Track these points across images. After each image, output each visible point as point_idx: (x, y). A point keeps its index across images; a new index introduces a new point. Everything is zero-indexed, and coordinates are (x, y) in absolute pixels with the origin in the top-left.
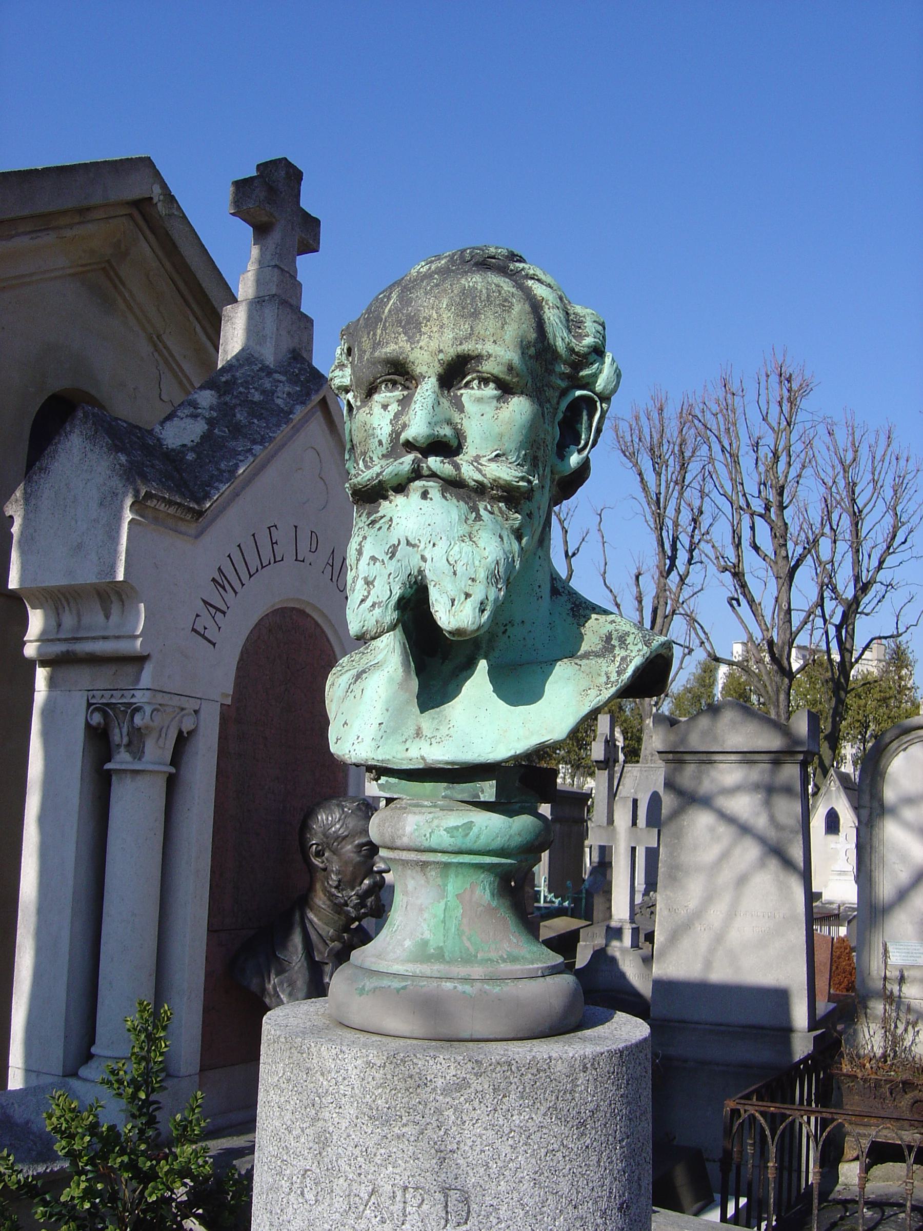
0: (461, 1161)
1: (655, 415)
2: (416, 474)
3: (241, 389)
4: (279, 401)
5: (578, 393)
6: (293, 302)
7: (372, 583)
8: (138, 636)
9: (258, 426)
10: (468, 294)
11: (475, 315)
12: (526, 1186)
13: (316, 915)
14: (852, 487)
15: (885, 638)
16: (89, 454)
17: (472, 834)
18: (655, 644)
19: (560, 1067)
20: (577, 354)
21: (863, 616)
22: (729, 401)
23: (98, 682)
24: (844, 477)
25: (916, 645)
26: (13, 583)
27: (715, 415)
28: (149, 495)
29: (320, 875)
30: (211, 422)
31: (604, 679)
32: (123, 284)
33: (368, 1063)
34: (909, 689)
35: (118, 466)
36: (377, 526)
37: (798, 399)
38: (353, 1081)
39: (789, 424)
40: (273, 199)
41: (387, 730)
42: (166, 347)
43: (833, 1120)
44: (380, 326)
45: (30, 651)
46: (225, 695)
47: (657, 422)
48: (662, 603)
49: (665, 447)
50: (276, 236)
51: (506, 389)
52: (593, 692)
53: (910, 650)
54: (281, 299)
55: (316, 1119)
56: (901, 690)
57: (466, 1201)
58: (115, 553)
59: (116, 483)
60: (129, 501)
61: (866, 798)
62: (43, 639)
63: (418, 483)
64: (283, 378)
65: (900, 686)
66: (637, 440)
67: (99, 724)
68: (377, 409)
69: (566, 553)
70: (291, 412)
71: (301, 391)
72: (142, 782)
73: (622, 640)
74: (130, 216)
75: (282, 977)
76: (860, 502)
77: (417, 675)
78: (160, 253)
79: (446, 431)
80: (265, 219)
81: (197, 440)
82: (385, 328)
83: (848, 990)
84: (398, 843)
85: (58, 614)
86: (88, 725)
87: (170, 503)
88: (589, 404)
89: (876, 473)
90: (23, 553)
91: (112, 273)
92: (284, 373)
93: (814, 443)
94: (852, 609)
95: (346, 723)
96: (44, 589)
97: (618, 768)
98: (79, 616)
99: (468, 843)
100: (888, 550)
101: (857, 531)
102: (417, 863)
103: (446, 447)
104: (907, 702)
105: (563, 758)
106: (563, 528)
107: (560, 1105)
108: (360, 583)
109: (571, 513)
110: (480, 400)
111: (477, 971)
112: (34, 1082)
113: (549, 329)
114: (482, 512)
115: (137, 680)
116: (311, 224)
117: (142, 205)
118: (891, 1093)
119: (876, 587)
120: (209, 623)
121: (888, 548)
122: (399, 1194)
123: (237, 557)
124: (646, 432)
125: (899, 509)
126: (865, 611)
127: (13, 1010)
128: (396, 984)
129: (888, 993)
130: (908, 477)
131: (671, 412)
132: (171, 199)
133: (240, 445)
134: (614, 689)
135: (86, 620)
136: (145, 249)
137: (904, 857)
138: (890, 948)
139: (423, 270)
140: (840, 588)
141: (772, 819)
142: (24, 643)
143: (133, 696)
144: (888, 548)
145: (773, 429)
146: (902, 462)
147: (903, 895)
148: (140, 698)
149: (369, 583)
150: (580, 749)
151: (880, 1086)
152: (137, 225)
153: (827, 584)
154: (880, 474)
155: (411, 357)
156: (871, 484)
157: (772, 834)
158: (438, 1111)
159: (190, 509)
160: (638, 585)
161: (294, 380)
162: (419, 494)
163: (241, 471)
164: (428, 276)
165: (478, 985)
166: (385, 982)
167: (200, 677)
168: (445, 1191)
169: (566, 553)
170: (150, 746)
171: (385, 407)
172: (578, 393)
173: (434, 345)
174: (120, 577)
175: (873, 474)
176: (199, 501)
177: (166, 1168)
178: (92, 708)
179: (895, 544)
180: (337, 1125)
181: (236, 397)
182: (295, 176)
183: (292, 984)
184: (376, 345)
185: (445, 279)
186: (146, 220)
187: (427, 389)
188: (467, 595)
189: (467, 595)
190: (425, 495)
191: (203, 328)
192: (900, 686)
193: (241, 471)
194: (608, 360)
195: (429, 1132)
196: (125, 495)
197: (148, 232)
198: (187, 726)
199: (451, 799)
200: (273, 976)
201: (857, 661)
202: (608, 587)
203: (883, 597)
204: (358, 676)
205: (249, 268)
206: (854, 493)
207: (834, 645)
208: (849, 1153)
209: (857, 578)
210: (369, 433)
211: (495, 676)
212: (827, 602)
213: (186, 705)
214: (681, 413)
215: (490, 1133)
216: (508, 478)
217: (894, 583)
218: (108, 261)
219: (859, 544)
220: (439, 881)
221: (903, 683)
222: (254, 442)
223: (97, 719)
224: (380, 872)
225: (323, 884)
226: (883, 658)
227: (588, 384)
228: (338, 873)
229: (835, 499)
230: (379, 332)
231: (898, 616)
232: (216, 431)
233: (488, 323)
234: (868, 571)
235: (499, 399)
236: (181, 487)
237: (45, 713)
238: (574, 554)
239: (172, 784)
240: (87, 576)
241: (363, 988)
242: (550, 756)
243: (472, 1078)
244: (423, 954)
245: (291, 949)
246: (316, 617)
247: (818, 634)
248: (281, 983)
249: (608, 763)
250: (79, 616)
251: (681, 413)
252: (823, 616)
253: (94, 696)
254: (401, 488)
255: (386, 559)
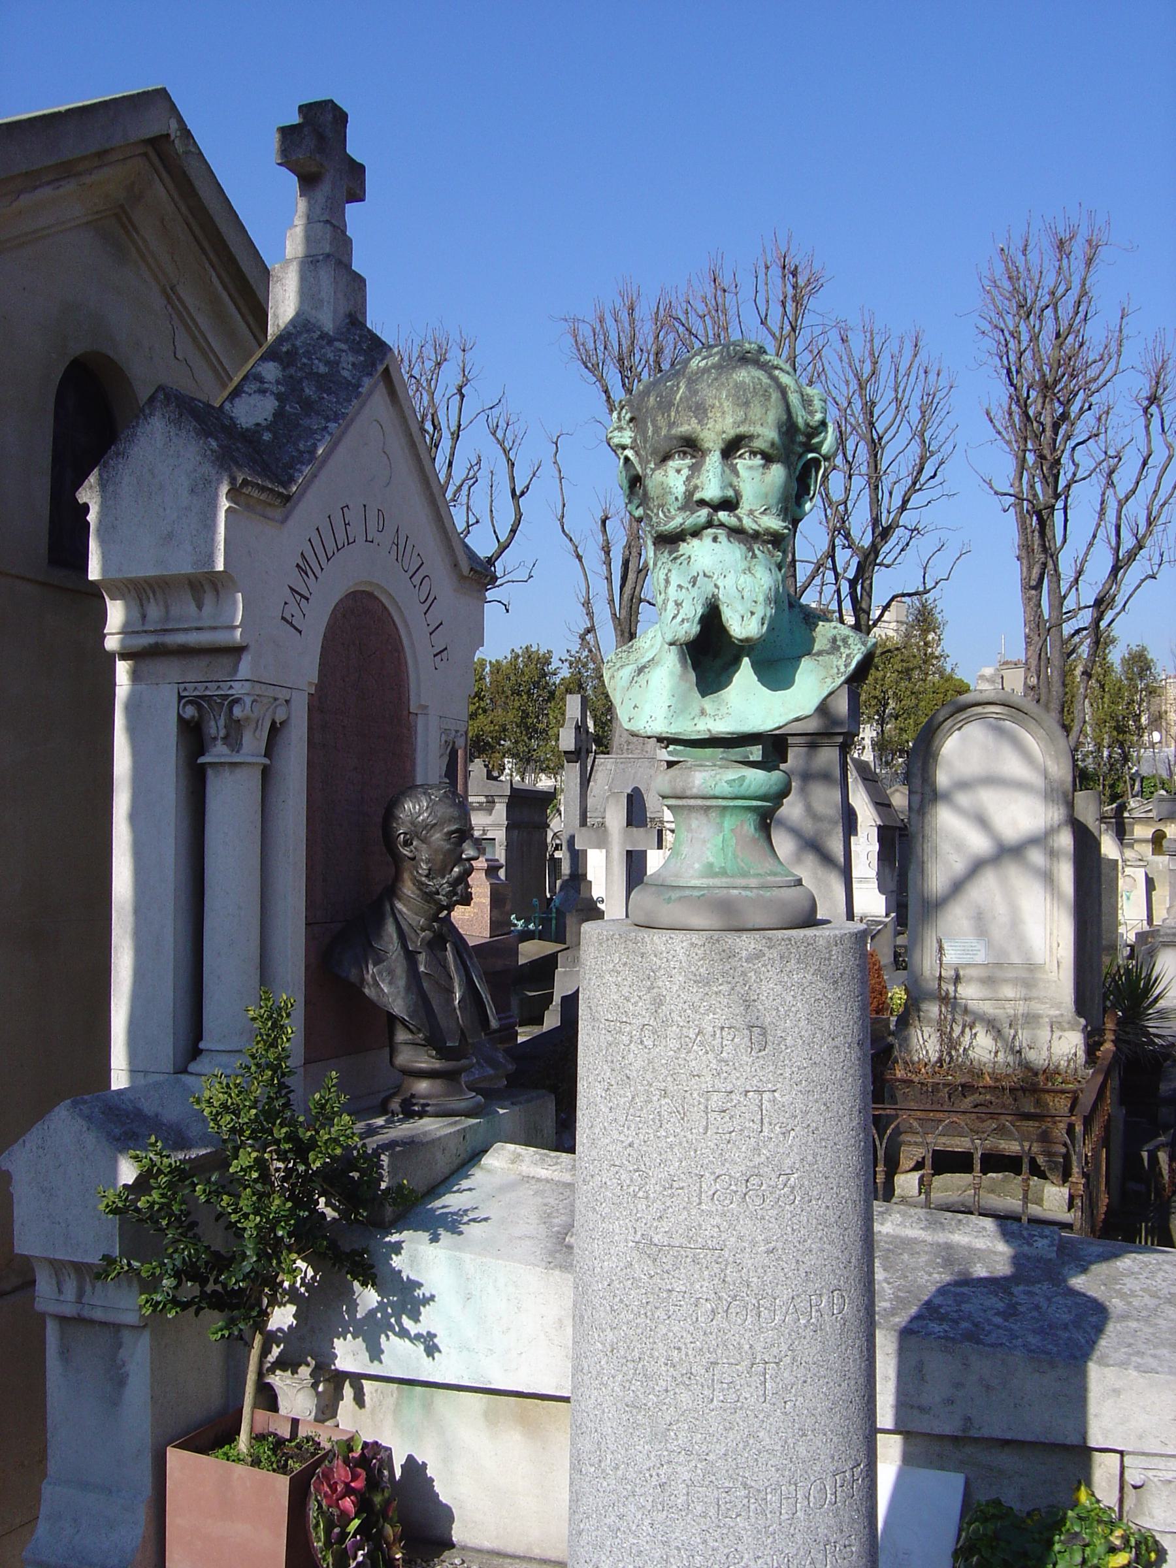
0: (760, 1007)
1: (624, 316)
2: (709, 524)
3: (305, 360)
4: (345, 373)
5: (810, 456)
6: (345, 259)
7: (681, 604)
8: (238, 627)
9: (329, 401)
10: (739, 386)
11: (747, 404)
12: (803, 1023)
13: (405, 905)
14: (869, 408)
15: (909, 595)
16: (174, 440)
17: (745, 784)
18: (869, 644)
19: (821, 942)
20: (811, 427)
21: (883, 568)
22: (720, 300)
23: (194, 673)
24: (861, 395)
25: (944, 603)
26: (94, 572)
27: (702, 317)
28: (245, 483)
29: (407, 864)
30: (279, 397)
31: (835, 670)
32: (137, 233)
33: (692, 944)
34: (937, 657)
35: (209, 452)
36: (679, 561)
37: (806, 298)
38: (681, 957)
39: (794, 329)
40: (318, 148)
41: (675, 712)
42: (179, 299)
43: (897, 1116)
44: (673, 410)
45: (112, 643)
46: (310, 683)
47: (627, 325)
48: (635, 553)
49: (637, 357)
50: (325, 188)
51: (768, 459)
52: (829, 680)
53: (938, 610)
54: (331, 257)
55: (650, 989)
56: (928, 659)
57: (764, 1034)
58: (212, 541)
59: (208, 469)
60: (224, 489)
61: (917, 781)
62: (126, 631)
63: (709, 530)
64: (344, 346)
65: (925, 654)
66: (602, 348)
67: (193, 717)
68: (672, 473)
69: (513, 491)
70: (360, 386)
71: (365, 361)
72: (240, 774)
73: (845, 640)
74: (145, 155)
75: (381, 966)
76: (880, 427)
77: (694, 669)
78: (176, 196)
79: (730, 493)
80: (314, 169)
81: (270, 418)
82: (677, 412)
83: (877, 1013)
84: (688, 793)
85: (142, 606)
86: (180, 718)
87: (263, 489)
88: (816, 463)
89: (900, 390)
90: (102, 542)
91: (124, 219)
92: (346, 342)
93: (823, 353)
94: (868, 561)
95: (636, 706)
96: (131, 580)
97: (590, 761)
98: (167, 607)
99: (742, 791)
100: (914, 488)
101: (876, 462)
102: (701, 807)
103: (729, 504)
104: (934, 673)
105: (509, 750)
106: (509, 460)
107: (823, 968)
108: (671, 605)
109: (518, 441)
110: (751, 468)
111: (753, 882)
112: (141, 1081)
113: (793, 410)
114: (757, 552)
115: (235, 669)
116: (357, 171)
117: (159, 143)
118: (950, 1098)
119: (899, 532)
120: (295, 610)
121: (914, 484)
122: (718, 1032)
123: (316, 541)
124: (613, 336)
125: (927, 435)
126: (885, 562)
127: (113, 1013)
128: (696, 893)
129: (943, 993)
130: (939, 395)
131: (645, 311)
132: (187, 134)
133: (315, 423)
134: (843, 678)
135: (175, 610)
136: (160, 192)
137: (959, 846)
138: (945, 946)
139: (702, 364)
140: (855, 533)
141: (809, 809)
142: (104, 636)
143: (231, 687)
144: (914, 484)
145: (773, 335)
146: (932, 376)
147: (958, 887)
148: (238, 690)
149: (678, 604)
150: (530, 739)
151: (938, 1091)
152: (152, 164)
153: (840, 529)
154: (904, 391)
155: (702, 436)
156: (894, 404)
157: (808, 827)
158: (744, 974)
159: (280, 494)
160: (604, 531)
161: (356, 349)
162: (710, 539)
163: (320, 452)
164: (706, 370)
165: (755, 891)
166: (687, 893)
167: (284, 666)
168: (750, 1027)
169: (513, 491)
170: (247, 738)
171: (678, 471)
172: (810, 456)
173: (718, 427)
174: (220, 566)
175: (896, 391)
176: (286, 484)
177: (327, 1137)
178: (183, 701)
179: (922, 479)
180: (669, 990)
181: (301, 369)
182: (340, 118)
183: (391, 972)
184: (671, 425)
185: (720, 374)
186: (162, 160)
187: (713, 460)
188: (752, 613)
189: (752, 613)
190: (715, 539)
191: (219, 277)
192: (925, 654)
193: (320, 452)
194: (830, 430)
195: (738, 988)
196: (219, 481)
197: (164, 175)
198: (280, 717)
199: (726, 759)
200: (370, 967)
201: (875, 625)
202: (566, 535)
203: (907, 544)
204: (641, 670)
205: (296, 222)
206: (872, 415)
207: (847, 605)
208: (906, 1163)
209: (876, 521)
210: (666, 491)
211: (757, 667)
212: (838, 550)
213: (280, 696)
214: (657, 313)
215: (779, 987)
216: (776, 527)
217: (920, 527)
218: (122, 207)
219: (879, 479)
220: (718, 820)
221: (930, 650)
222: (328, 419)
223: (190, 712)
224: (469, 860)
225: (412, 873)
226: (904, 619)
227: (816, 449)
228: (428, 861)
229: (851, 424)
230: (673, 414)
231: (925, 568)
232: (287, 408)
233: (756, 411)
234: (889, 512)
235: (764, 466)
236: (265, 470)
237: (130, 708)
238: (523, 494)
239: (266, 774)
240: (182, 565)
241: (670, 898)
242: (492, 747)
243: (766, 950)
244: (709, 871)
245: (386, 938)
246: (384, 601)
247: (829, 590)
248: (380, 973)
249: (577, 755)
250: (167, 607)
251: (657, 313)
252: (834, 569)
253: (185, 689)
254: (696, 533)
255: (690, 587)
